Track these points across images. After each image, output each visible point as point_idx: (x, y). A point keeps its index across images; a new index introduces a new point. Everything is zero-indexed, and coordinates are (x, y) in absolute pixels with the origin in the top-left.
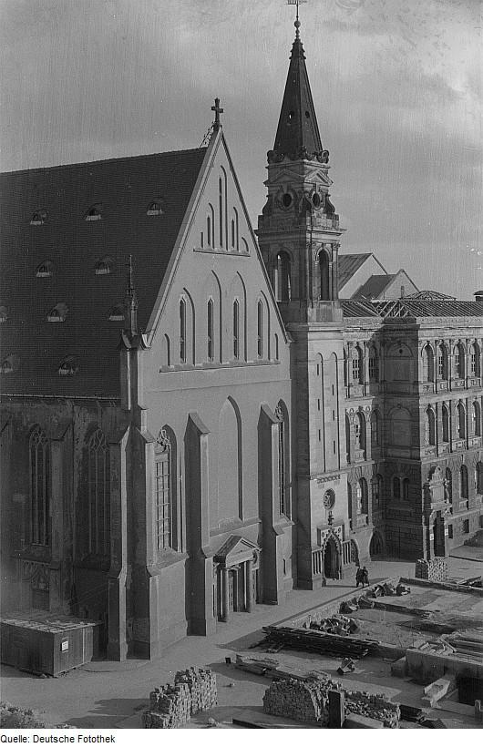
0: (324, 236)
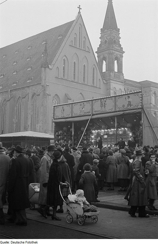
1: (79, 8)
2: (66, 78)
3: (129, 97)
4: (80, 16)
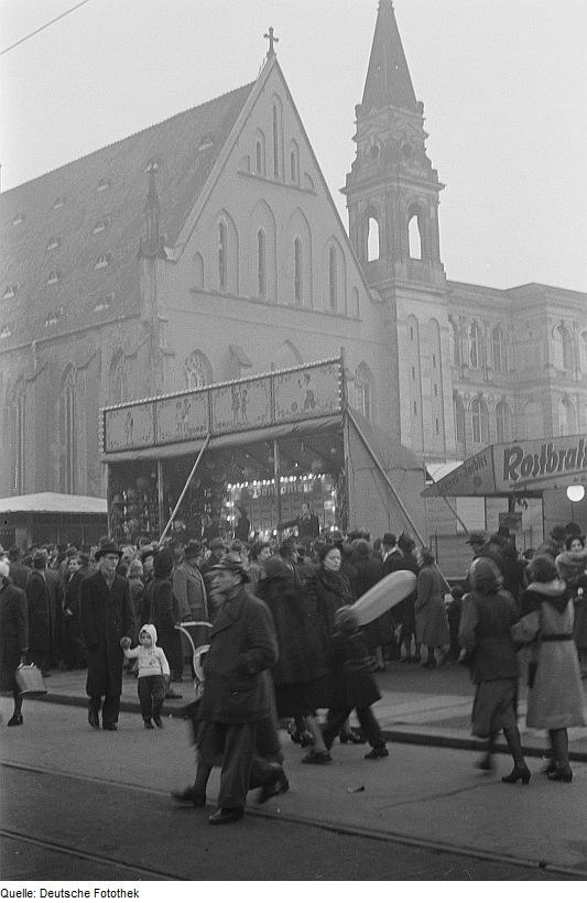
0: (416, 188)
1: (271, 37)
2: (230, 288)
3: (308, 377)
4: (272, 66)
